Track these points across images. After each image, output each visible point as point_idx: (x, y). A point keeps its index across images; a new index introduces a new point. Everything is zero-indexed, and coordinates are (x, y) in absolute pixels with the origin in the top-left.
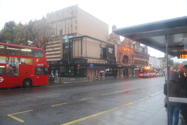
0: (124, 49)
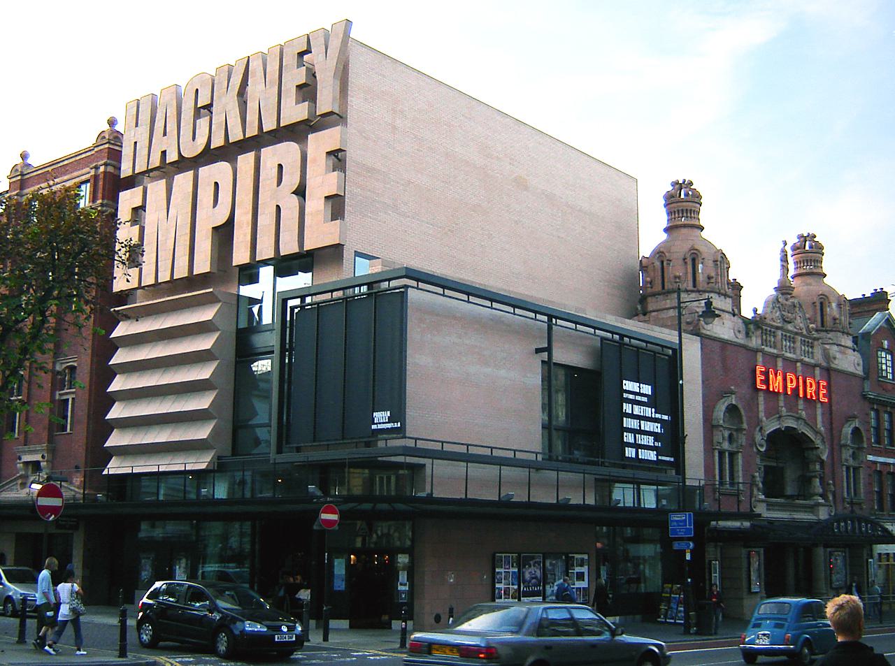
0: (766, 382)
